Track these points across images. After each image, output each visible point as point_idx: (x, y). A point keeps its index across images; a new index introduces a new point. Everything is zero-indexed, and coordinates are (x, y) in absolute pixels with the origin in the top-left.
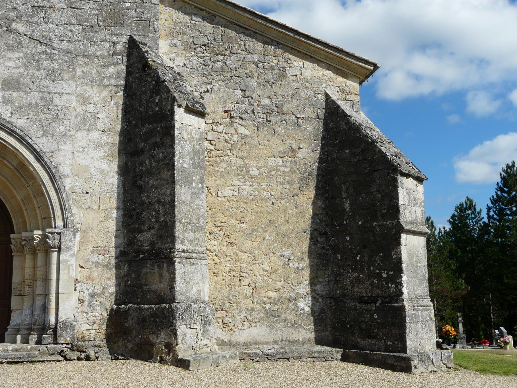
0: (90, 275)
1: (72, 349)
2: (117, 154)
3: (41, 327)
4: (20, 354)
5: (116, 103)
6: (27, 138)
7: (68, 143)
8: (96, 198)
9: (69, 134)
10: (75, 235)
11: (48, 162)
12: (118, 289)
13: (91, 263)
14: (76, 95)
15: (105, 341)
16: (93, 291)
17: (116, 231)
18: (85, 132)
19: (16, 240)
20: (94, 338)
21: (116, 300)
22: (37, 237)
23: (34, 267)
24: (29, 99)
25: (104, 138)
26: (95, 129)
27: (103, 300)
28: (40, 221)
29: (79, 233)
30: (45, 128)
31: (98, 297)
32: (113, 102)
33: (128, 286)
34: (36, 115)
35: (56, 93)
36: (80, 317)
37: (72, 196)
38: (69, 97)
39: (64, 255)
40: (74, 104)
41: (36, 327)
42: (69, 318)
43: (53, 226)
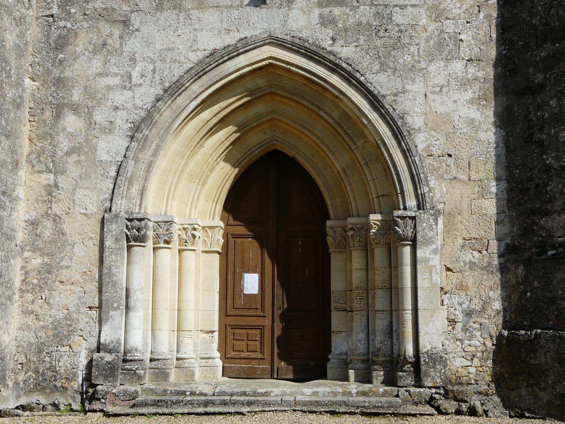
0: (462, 281)
1: (446, 395)
2: (492, 95)
3: (388, 359)
4: (377, 402)
5: (486, 17)
6: (358, 75)
7: (417, 81)
8: (465, 163)
9: (418, 66)
10: (437, 220)
11: (391, 110)
12: (506, 304)
13: (462, 264)
14: (426, 7)
15: (493, 385)
16: (469, 306)
17: (498, 213)
18: (443, 64)
19: (335, 229)
20: (476, 380)
21: (504, 321)
22: (375, 224)
23: (368, 268)
24: (357, 16)
25: (472, 70)
26: (455, 59)
27: (484, 321)
28: (376, 200)
29: (442, 217)
30: (383, 59)
31: (477, 317)
32: (482, 15)
33: (527, 300)
34: (368, 40)
35: (397, 6)
36: (451, 346)
37: (429, 161)
38: (415, 10)
39: (422, 250)
40: (423, 22)
41: (381, 359)
42: (435, 348)
43: (402, 207)
